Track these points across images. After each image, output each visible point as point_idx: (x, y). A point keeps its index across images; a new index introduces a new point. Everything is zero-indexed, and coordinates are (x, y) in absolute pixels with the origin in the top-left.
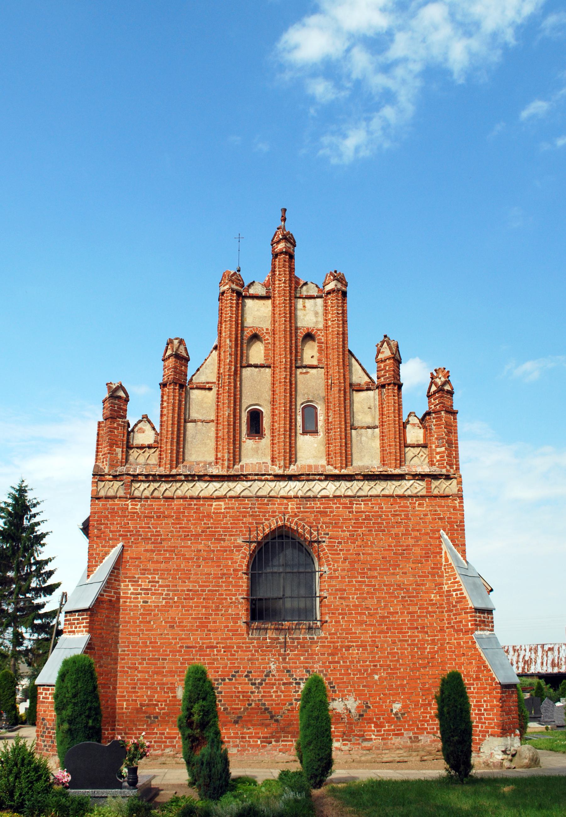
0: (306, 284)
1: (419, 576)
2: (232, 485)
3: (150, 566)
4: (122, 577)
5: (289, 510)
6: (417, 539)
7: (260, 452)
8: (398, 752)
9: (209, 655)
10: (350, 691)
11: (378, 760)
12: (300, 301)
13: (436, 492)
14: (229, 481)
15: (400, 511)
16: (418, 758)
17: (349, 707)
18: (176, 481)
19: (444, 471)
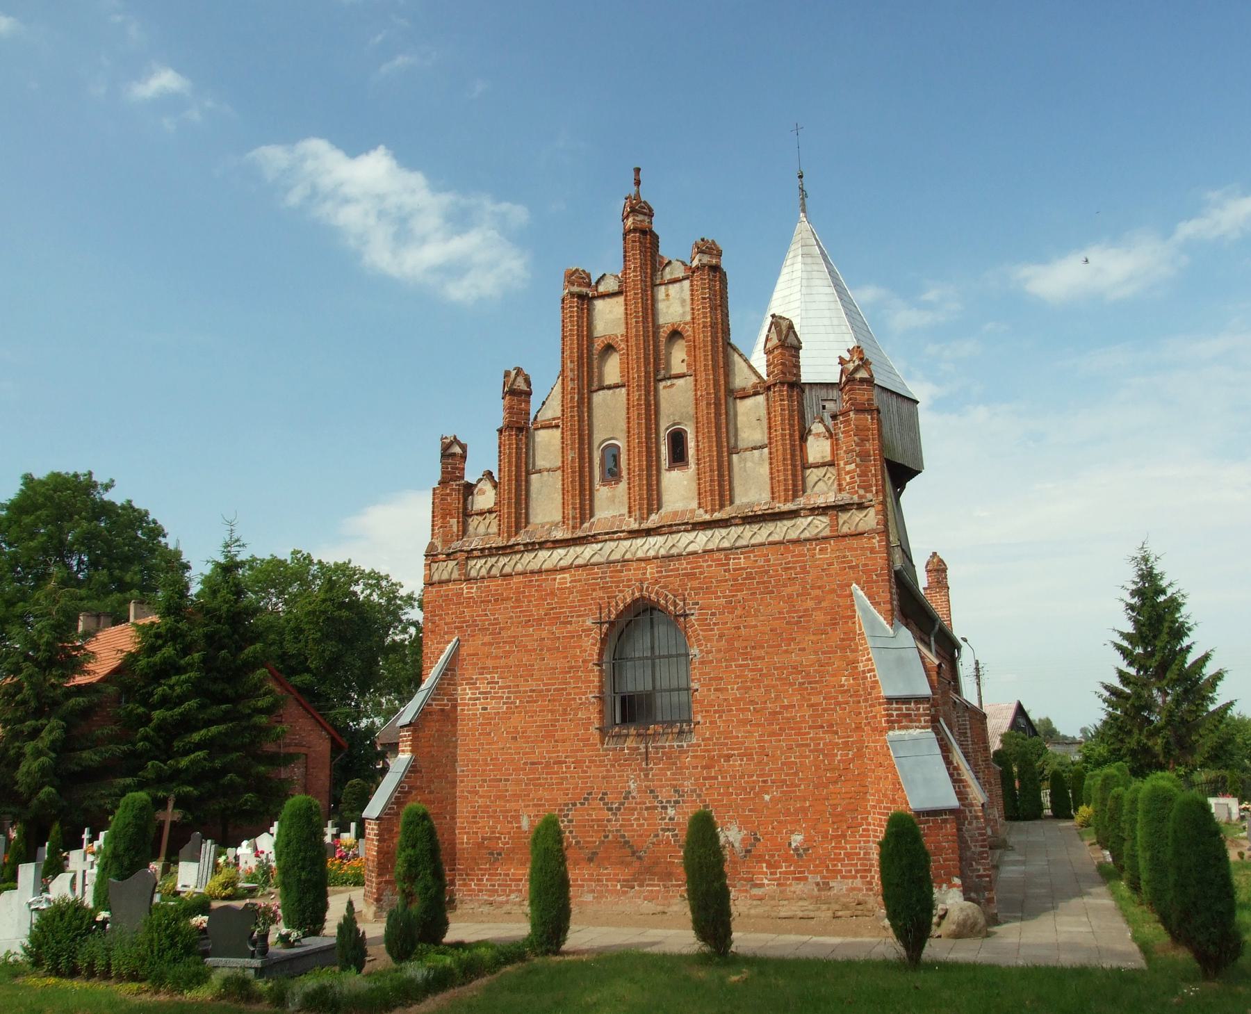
0: (670, 263)
1: (824, 653)
2: (579, 549)
3: (489, 663)
4: (458, 678)
5: (648, 576)
6: (819, 600)
7: (617, 500)
8: (801, 903)
9: (557, 773)
10: (731, 817)
11: (773, 914)
12: (662, 288)
13: (845, 530)
14: (576, 545)
15: (794, 562)
16: (830, 914)
17: (731, 839)
18: (516, 553)
19: (856, 499)
